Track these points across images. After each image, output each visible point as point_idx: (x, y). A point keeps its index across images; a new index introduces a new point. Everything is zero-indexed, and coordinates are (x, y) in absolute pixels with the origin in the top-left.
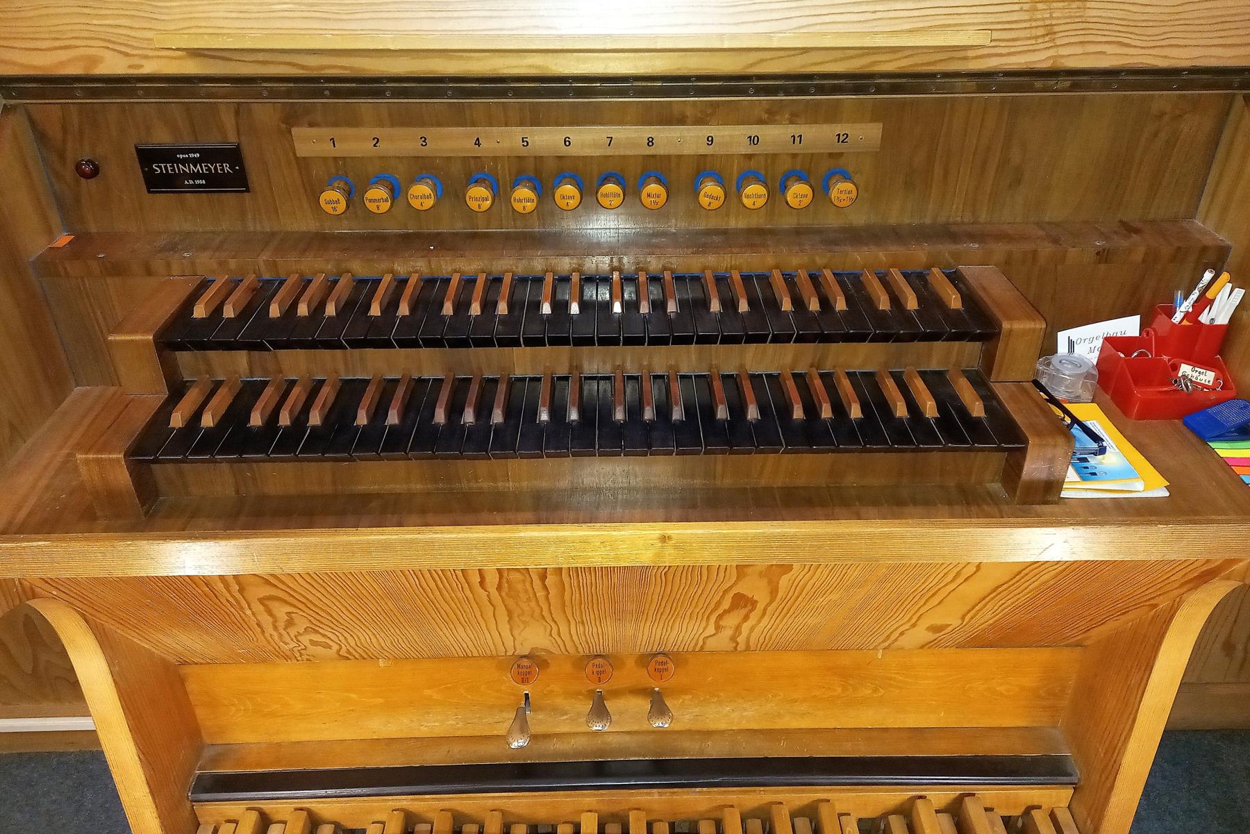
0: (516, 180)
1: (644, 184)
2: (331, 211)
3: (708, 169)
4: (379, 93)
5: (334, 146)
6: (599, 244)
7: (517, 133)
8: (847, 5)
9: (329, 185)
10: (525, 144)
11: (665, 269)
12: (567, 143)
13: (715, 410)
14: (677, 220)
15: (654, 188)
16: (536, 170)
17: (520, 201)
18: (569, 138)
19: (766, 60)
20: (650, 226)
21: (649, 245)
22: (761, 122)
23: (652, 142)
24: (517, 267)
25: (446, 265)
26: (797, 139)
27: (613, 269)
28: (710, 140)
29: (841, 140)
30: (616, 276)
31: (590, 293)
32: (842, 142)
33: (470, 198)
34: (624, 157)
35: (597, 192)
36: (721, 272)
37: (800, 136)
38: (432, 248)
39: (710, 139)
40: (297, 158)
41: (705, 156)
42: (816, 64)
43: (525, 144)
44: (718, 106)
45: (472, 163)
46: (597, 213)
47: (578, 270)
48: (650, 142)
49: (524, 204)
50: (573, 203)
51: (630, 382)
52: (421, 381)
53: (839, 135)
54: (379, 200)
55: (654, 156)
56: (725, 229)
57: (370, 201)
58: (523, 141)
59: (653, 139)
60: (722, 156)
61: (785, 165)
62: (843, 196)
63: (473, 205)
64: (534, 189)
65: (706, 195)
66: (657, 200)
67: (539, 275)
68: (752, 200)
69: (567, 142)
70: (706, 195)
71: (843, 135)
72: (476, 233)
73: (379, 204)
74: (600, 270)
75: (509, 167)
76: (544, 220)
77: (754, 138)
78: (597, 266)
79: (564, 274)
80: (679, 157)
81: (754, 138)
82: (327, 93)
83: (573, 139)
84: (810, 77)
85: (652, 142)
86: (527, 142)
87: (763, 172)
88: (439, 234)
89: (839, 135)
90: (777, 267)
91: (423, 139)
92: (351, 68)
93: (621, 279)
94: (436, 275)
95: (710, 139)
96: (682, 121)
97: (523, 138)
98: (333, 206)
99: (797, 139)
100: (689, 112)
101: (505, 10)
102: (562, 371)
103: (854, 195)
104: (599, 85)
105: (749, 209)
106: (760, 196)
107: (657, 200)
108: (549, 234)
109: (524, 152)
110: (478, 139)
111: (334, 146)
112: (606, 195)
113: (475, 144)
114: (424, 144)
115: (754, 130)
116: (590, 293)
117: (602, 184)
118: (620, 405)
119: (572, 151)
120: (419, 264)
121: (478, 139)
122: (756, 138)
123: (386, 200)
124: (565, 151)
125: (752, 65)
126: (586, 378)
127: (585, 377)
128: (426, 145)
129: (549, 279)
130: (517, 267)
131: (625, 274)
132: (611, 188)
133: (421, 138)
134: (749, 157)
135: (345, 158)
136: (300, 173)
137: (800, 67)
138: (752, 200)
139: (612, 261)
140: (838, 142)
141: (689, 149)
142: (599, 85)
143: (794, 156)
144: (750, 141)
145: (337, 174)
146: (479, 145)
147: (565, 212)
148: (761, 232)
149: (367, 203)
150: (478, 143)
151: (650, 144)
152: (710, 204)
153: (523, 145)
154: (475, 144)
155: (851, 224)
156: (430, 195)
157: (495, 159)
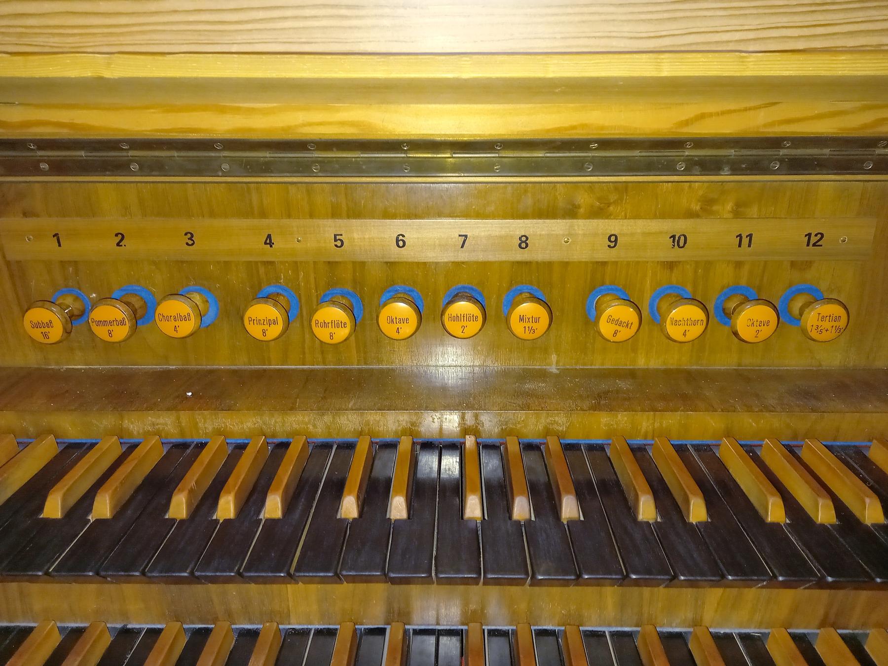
0: (324, 296)
1: (513, 304)
2: (40, 339)
3: (607, 283)
4: (121, 167)
5: (60, 245)
6: (444, 389)
7: (328, 228)
8: (835, 37)
9: (46, 302)
10: (339, 243)
11: (548, 432)
12: (401, 243)
13: (558, 509)
14: (558, 355)
15: (527, 308)
16: (355, 281)
17: (325, 325)
18: (403, 236)
19: (711, 115)
20: (517, 363)
21: (518, 394)
22: (690, 215)
23: (525, 242)
24: (315, 426)
25: (205, 422)
26: (745, 241)
27: (466, 431)
28: (613, 240)
29: (812, 242)
30: (470, 442)
31: (428, 462)
32: (814, 245)
33: (250, 319)
34: (485, 265)
35: (443, 314)
36: (638, 441)
37: (750, 236)
38: (190, 394)
39: (613, 239)
40: (8, 264)
41: (604, 264)
42: (788, 121)
43: (339, 243)
44: (626, 189)
45: (262, 270)
46: (442, 344)
47: (410, 432)
48: (523, 242)
49: (331, 329)
50: (407, 330)
51: (495, 640)
52: (126, 634)
53: (809, 235)
54: (111, 323)
55: (527, 264)
56: (630, 369)
57: (99, 323)
58: (336, 240)
59: (527, 238)
60: (628, 263)
61: (723, 276)
62: (827, 324)
63: (255, 331)
64: (349, 309)
65: (610, 320)
66: (535, 326)
67: (350, 438)
68: (682, 329)
69: (400, 242)
70: (610, 320)
71: (816, 235)
72: (265, 370)
73: (110, 328)
74: (445, 432)
75: (315, 278)
76: (365, 353)
77: (679, 238)
78: (441, 426)
79: (389, 438)
80: (565, 265)
81: (679, 238)
82: (44, 166)
83: (410, 237)
84: (776, 142)
85: (525, 242)
86: (341, 241)
87: (689, 288)
88: (211, 372)
89: (809, 235)
90: (728, 434)
91: (189, 236)
92: (71, 126)
93: (478, 444)
94: (188, 439)
95: (613, 239)
96: (571, 212)
97: (335, 236)
98: (43, 330)
99: (745, 241)
100: (584, 199)
101: (308, 43)
102: (374, 618)
103: (842, 323)
104: (448, 155)
105: (675, 341)
106: (695, 323)
107: (535, 326)
108: (371, 372)
109: (337, 255)
110: (269, 236)
111: (60, 245)
112: (457, 318)
113: (266, 243)
114: (190, 242)
115: (680, 226)
116: (428, 462)
117: (451, 302)
118: (473, 491)
119: (407, 254)
120: (161, 420)
121: (269, 236)
122: (682, 238)
123: (122, 323)
124: (396, 254)
125: (687, 123)
126: (417, 632)
127: (414, 630)
128: (193, 244)
129: (362, 448)
130: (315, 426)
131: (483, 439)
132: (463, 307)
133: (186, 234)
134: (671, 265)
135: (76, 262)
136: (14, 284)
137: (765, 126)
138: (682, 329)
139: (463, 418)
140: (808, 245)
141: (581, 253)
142: (448, 155)
143: (738, 265)
144: (674, 242)
145: (66, 286)
146: (271, 244)
147: (396, 343)
148: (690, 376)
149: (94, 328)
150: (269, 241)
151: (523, 245)
152: (615, 333)
153: (336, 246)
154: (266, 243)
155: (820, 365)
156: (189, 314)
157: (295, 265)
